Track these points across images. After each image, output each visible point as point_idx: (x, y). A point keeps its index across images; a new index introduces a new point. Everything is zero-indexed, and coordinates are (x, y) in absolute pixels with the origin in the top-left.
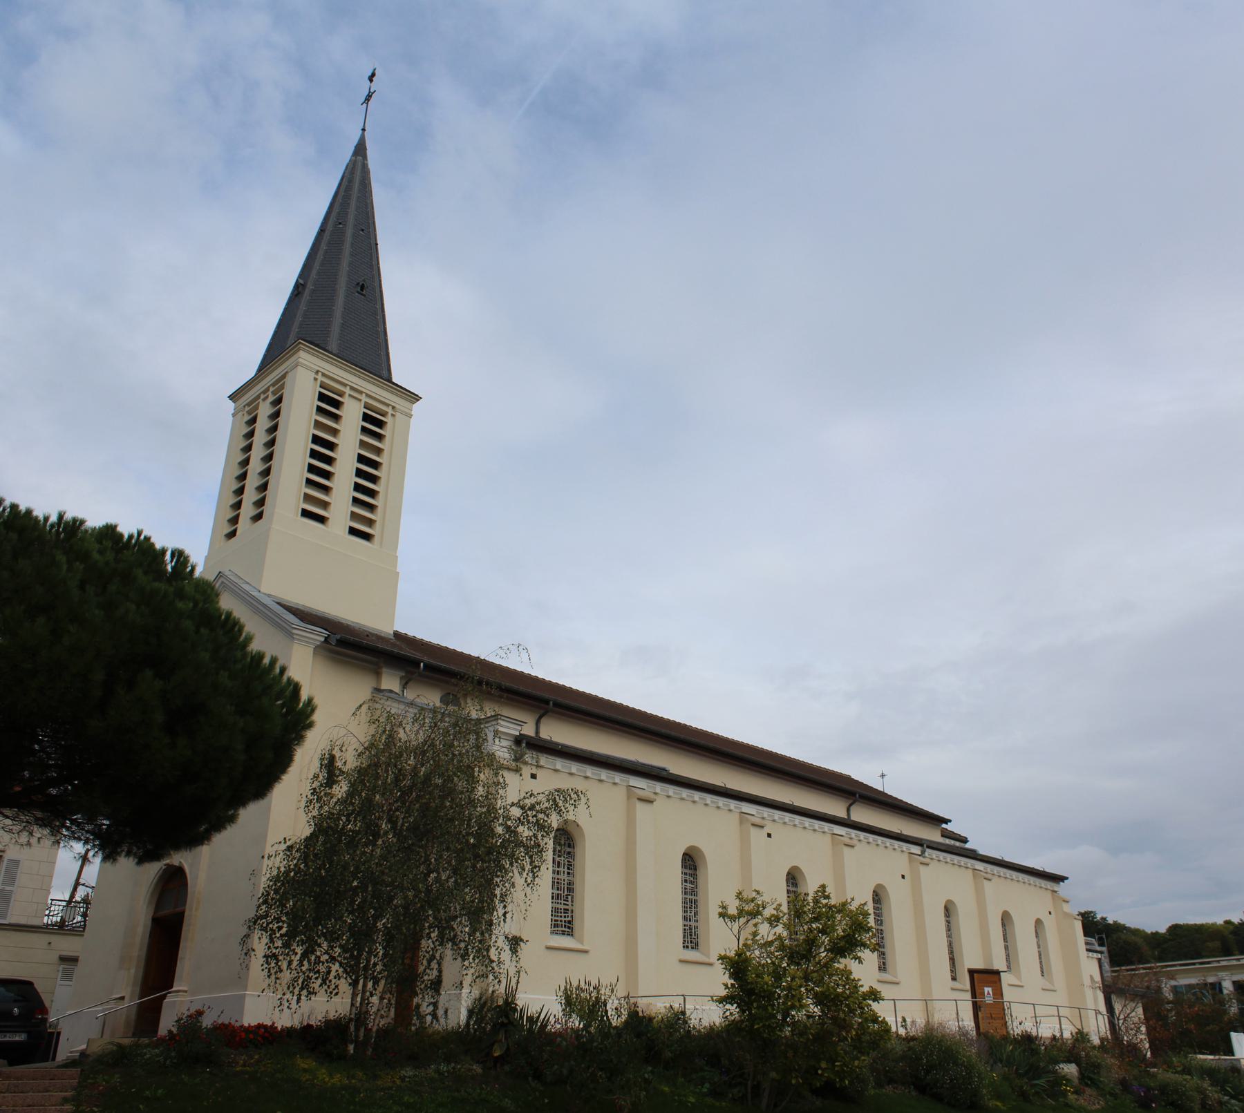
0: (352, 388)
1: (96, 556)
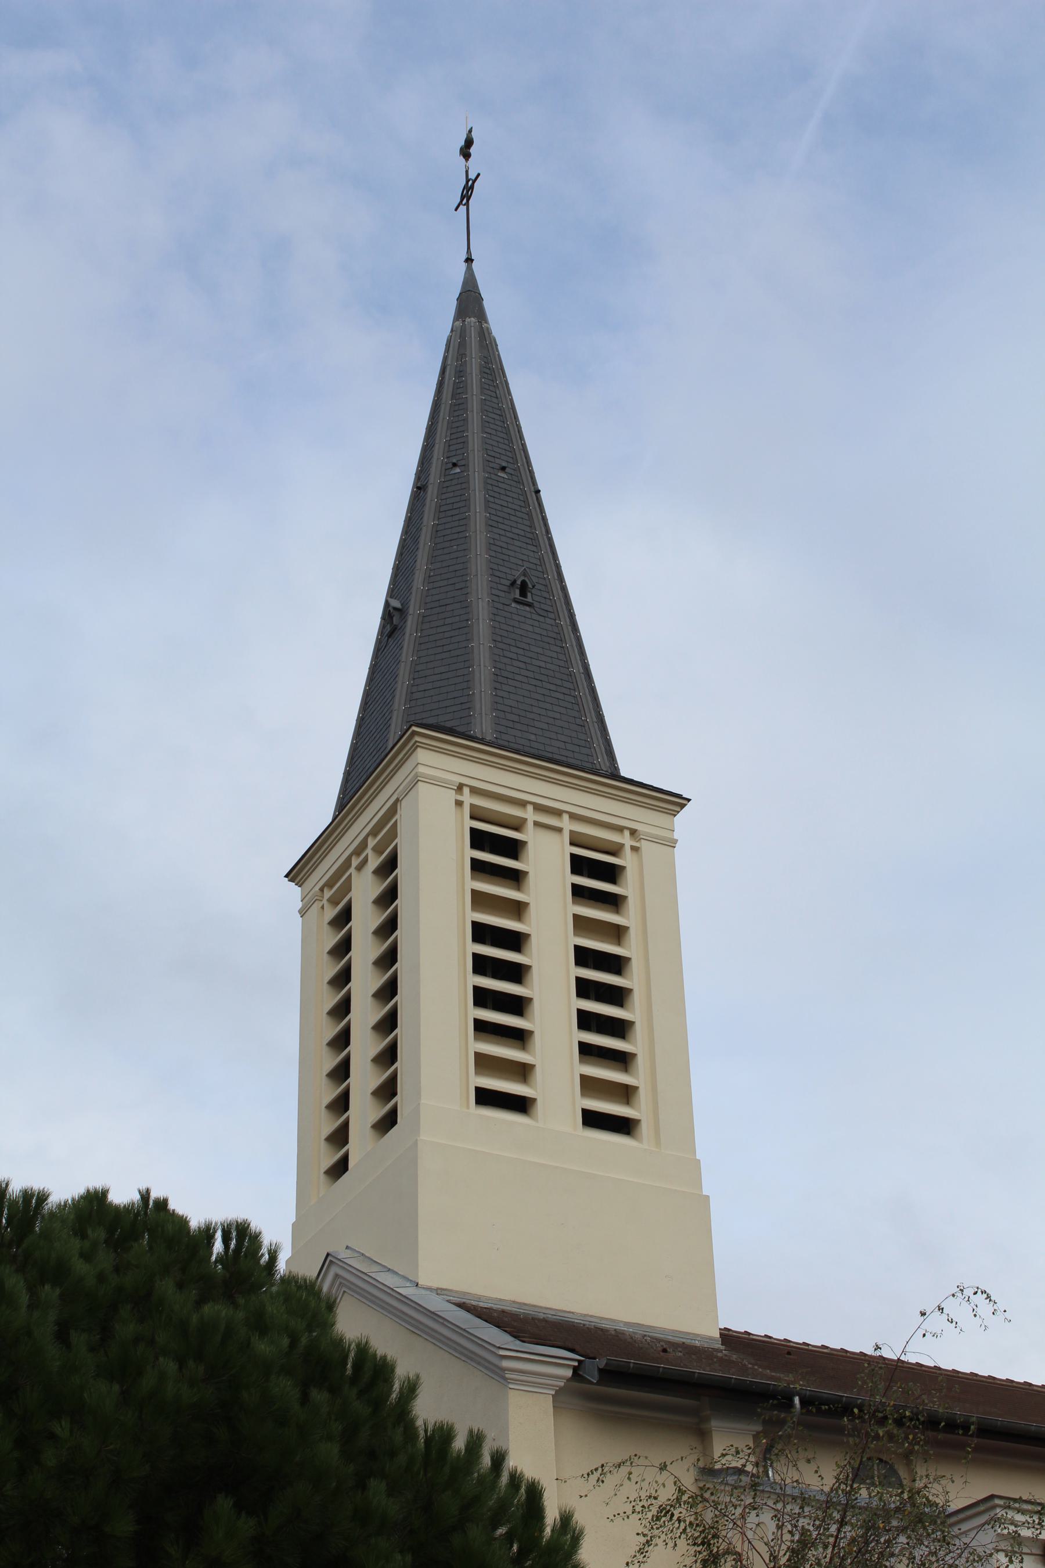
0: (539, 808)
1: (80, 1267)
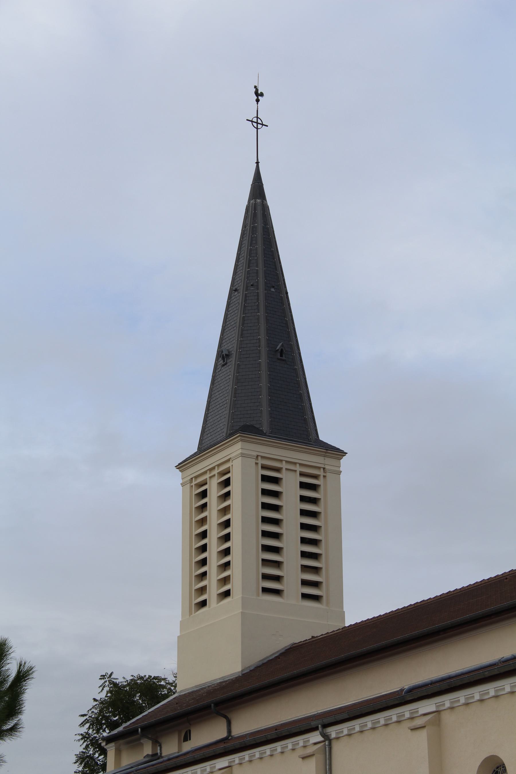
0: (287, 462)
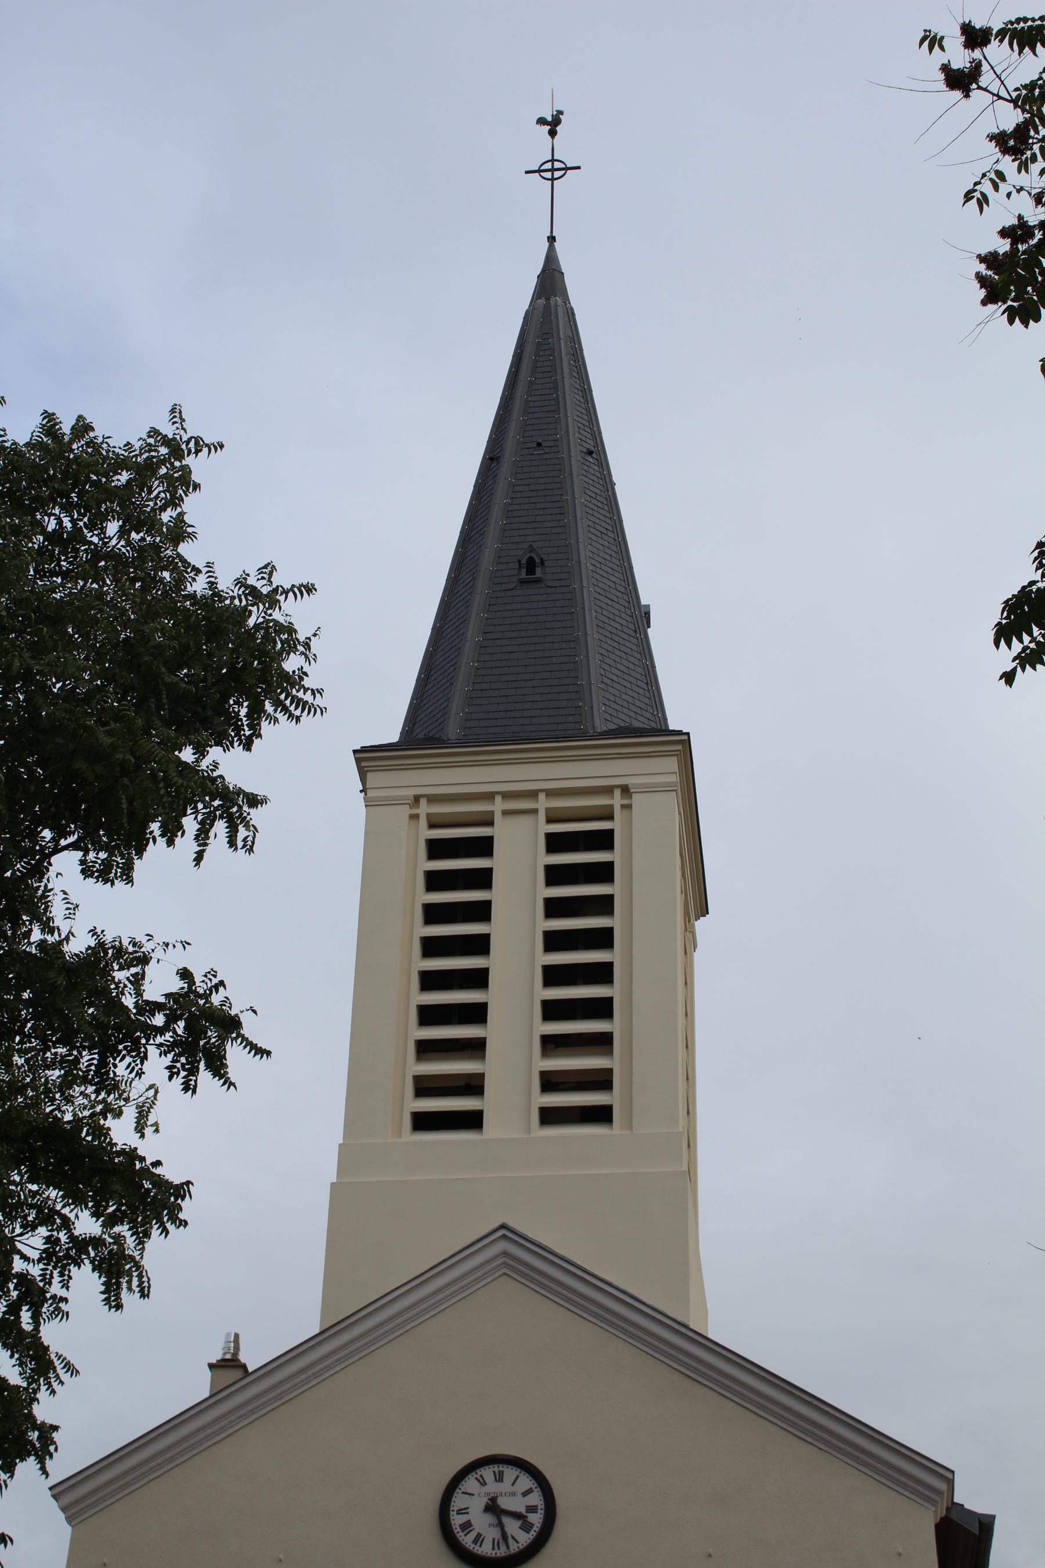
0: (507, 796)
